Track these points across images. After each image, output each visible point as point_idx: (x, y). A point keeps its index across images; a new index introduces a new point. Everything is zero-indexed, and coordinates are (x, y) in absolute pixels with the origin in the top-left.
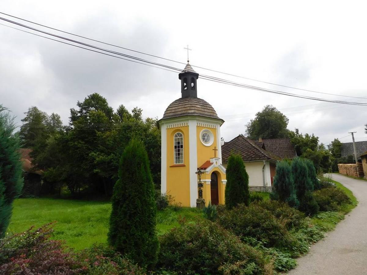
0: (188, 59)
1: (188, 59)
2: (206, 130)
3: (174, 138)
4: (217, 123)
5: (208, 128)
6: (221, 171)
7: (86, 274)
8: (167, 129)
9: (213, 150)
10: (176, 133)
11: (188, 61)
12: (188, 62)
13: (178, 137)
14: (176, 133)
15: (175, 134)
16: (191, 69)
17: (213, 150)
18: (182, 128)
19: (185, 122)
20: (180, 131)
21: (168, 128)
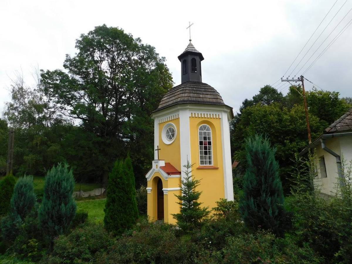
0: (190, 37)
1: (190, 37)
2: (167, 125)
3: (199, 131)
4: (221, 111)
5: (169, 121)
6: (152, 177)
7: (351, 204)
8: (159, 124)
9: (160, 149)
10: (202, 125)
11: (190, 40)
12: (189, 42)
13: (205, 131)
14: (202, 125)
15: (200, 126)
16: (193, 49)
17: (160, 149)
18: (211, 119)
19: (216, 113)
20: (208, 124)
21: (160, 122)
